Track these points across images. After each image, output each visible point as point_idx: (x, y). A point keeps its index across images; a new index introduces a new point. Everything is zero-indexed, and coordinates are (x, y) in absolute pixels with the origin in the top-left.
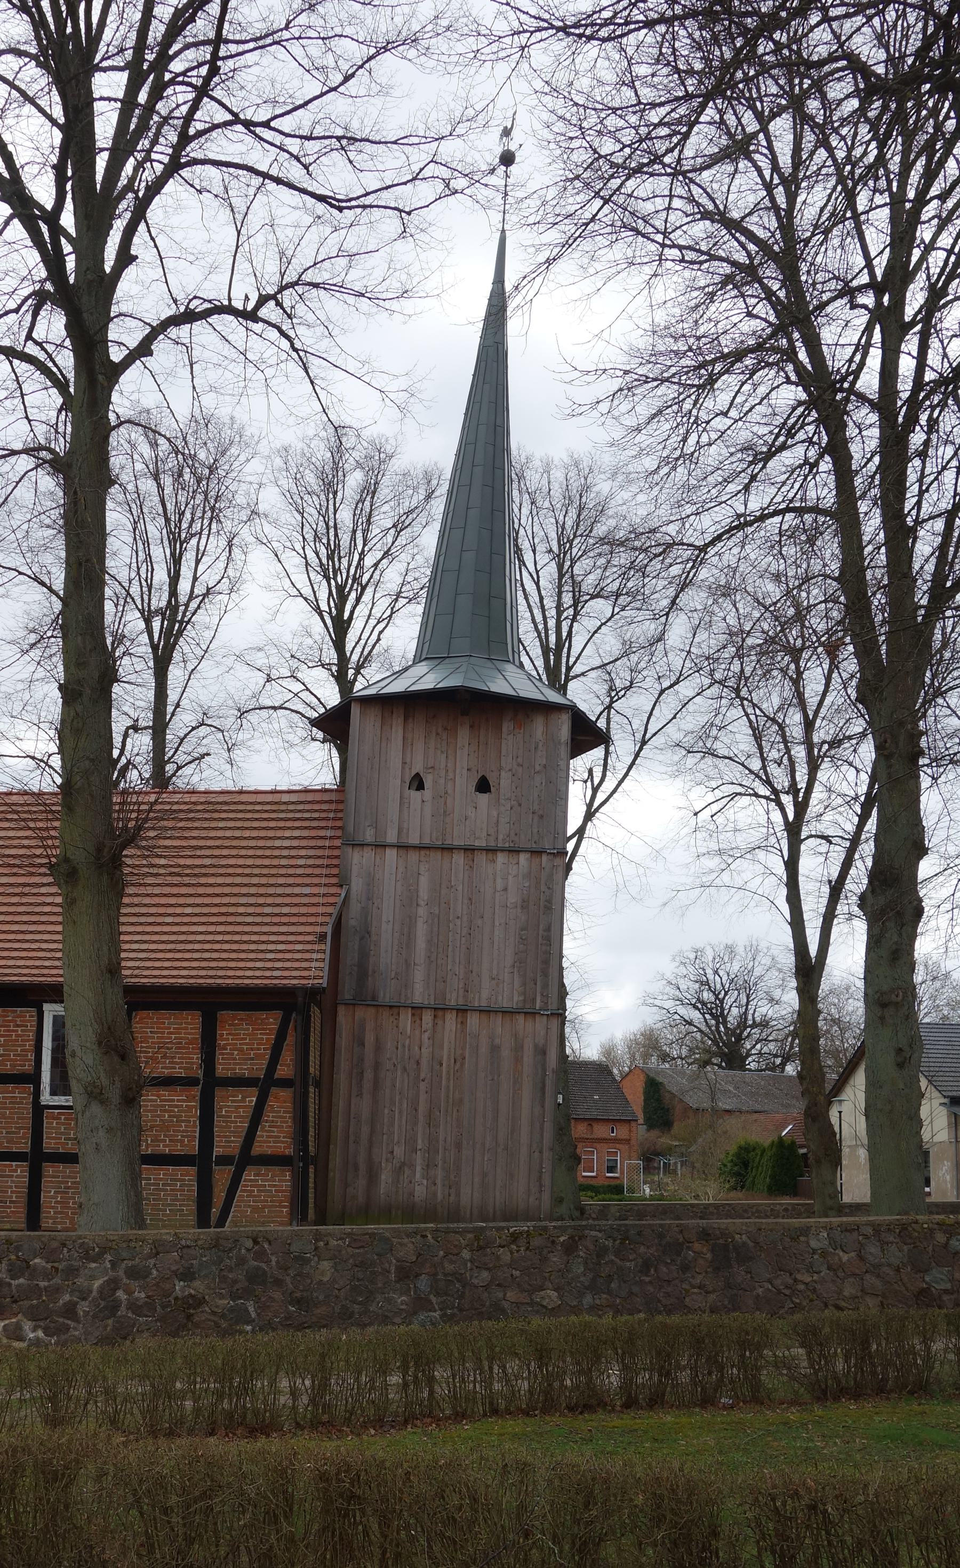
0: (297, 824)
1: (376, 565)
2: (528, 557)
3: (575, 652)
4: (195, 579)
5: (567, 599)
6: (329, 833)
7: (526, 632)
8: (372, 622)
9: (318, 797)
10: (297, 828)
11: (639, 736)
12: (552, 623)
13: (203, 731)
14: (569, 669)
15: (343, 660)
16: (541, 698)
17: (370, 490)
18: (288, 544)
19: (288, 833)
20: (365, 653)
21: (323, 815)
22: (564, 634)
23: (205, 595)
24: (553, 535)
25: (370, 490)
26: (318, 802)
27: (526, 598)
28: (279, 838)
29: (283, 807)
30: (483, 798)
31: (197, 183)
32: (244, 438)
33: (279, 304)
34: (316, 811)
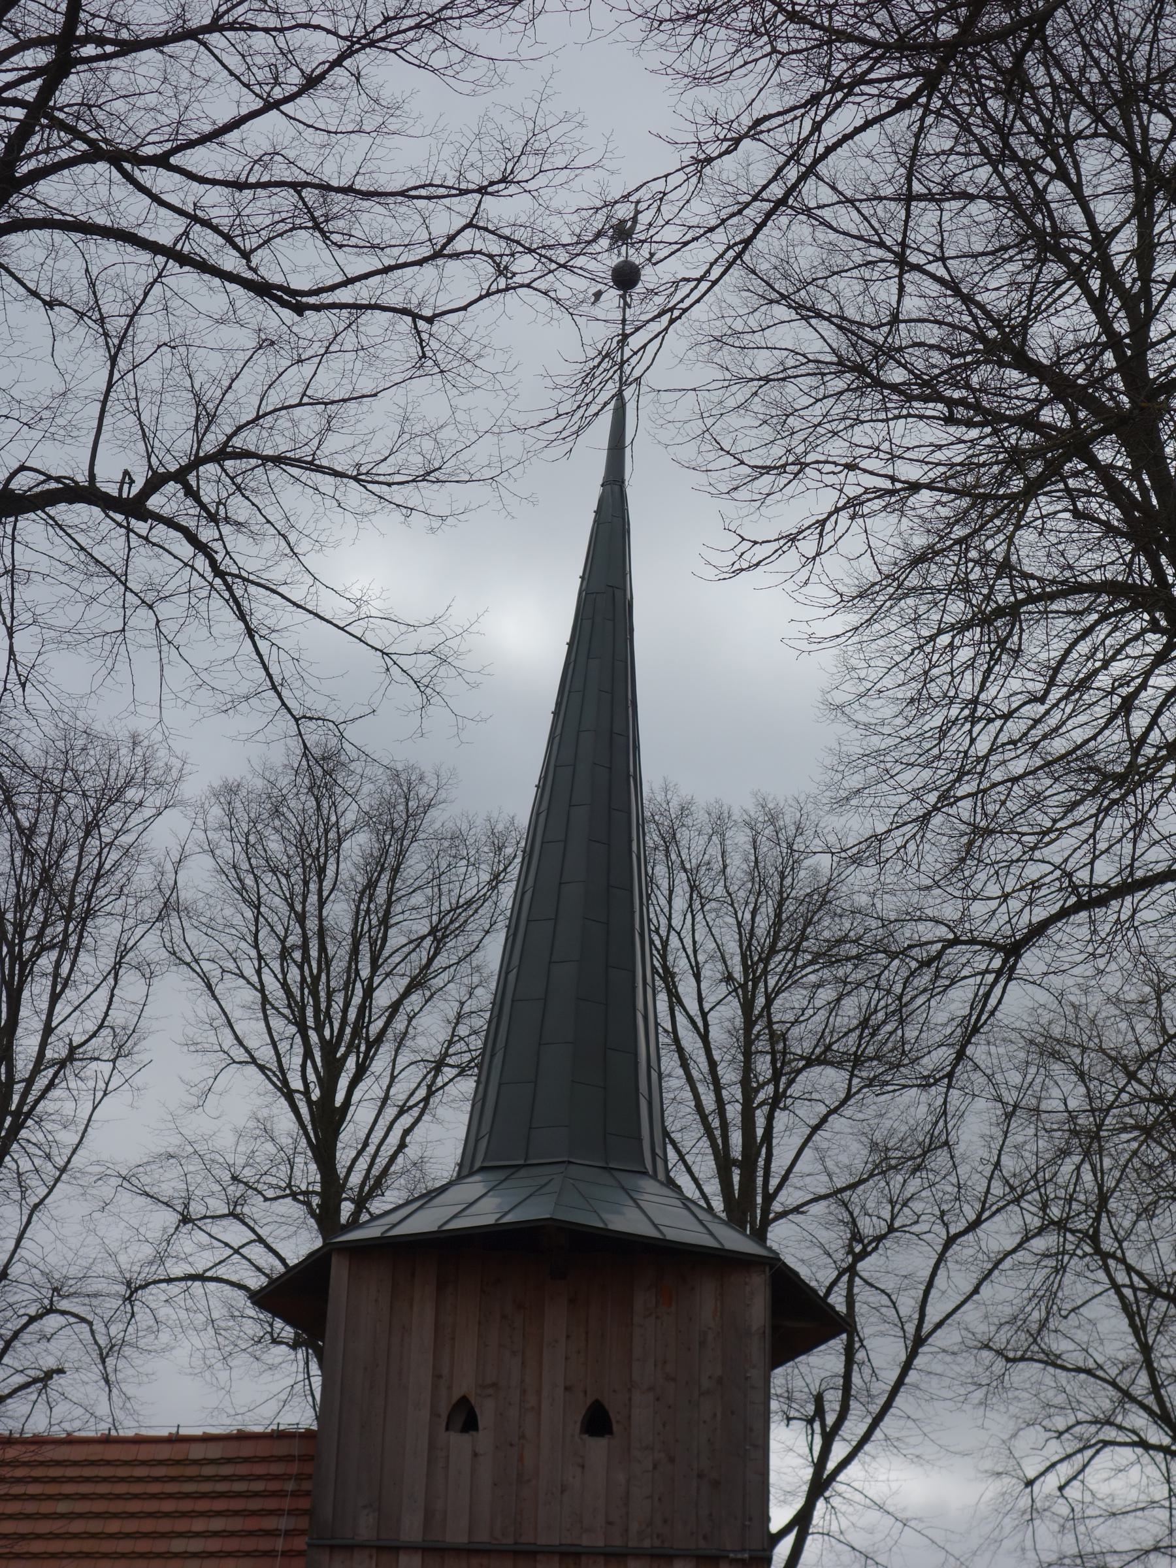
0: (220, 1505)
1: (395, 1007)
2: (686, 987)
3: (780, 1164)
4: (48, 1030)
5: (763, 1066)
6: (283, 1523)
7: (681, 1118)
8: (390, 1112)
9: (263, 1449)
10: (219, 1514)
11: (910, 1328)
12: (734, 1112)
13: (52, 1322)
14: (769, 1198)
15: (332, 1185)
16: (708, 1242)
17: (385, 866)
18: (231, 965)
19: (198, 1525)
20: (375, 1172)
21: (274, 1486)
22: (760, 1132)
23: (62, 1064)
24: (732, 948)
25: (385, 866)
26: (263, 1460)
27: (685, 1065)
28: (181, 1535)
29: (191, 1471)
30: (598, 1447)
31: (44, 290)
32: (153, 774)
33: (192, 493)
34: (259, 1478)
